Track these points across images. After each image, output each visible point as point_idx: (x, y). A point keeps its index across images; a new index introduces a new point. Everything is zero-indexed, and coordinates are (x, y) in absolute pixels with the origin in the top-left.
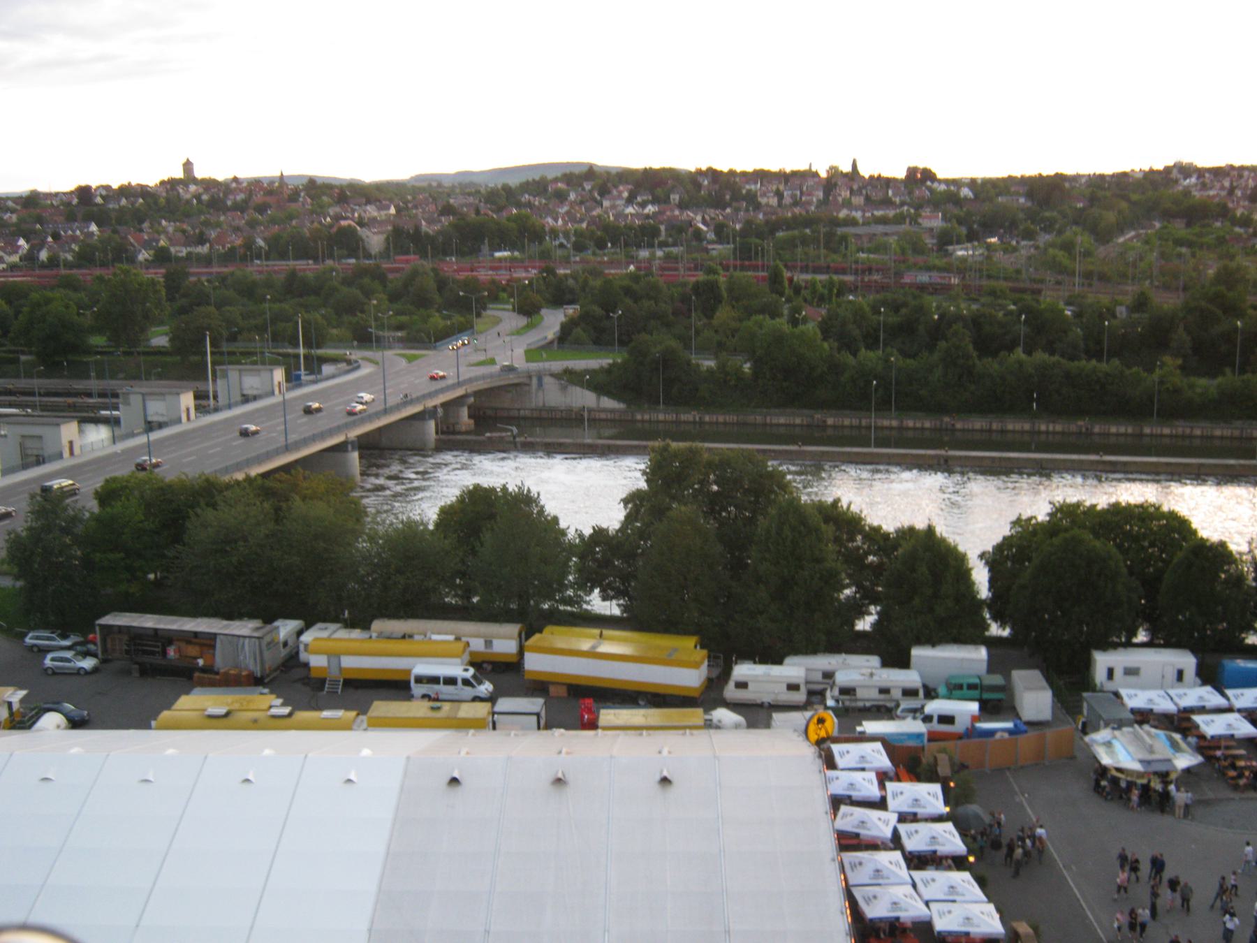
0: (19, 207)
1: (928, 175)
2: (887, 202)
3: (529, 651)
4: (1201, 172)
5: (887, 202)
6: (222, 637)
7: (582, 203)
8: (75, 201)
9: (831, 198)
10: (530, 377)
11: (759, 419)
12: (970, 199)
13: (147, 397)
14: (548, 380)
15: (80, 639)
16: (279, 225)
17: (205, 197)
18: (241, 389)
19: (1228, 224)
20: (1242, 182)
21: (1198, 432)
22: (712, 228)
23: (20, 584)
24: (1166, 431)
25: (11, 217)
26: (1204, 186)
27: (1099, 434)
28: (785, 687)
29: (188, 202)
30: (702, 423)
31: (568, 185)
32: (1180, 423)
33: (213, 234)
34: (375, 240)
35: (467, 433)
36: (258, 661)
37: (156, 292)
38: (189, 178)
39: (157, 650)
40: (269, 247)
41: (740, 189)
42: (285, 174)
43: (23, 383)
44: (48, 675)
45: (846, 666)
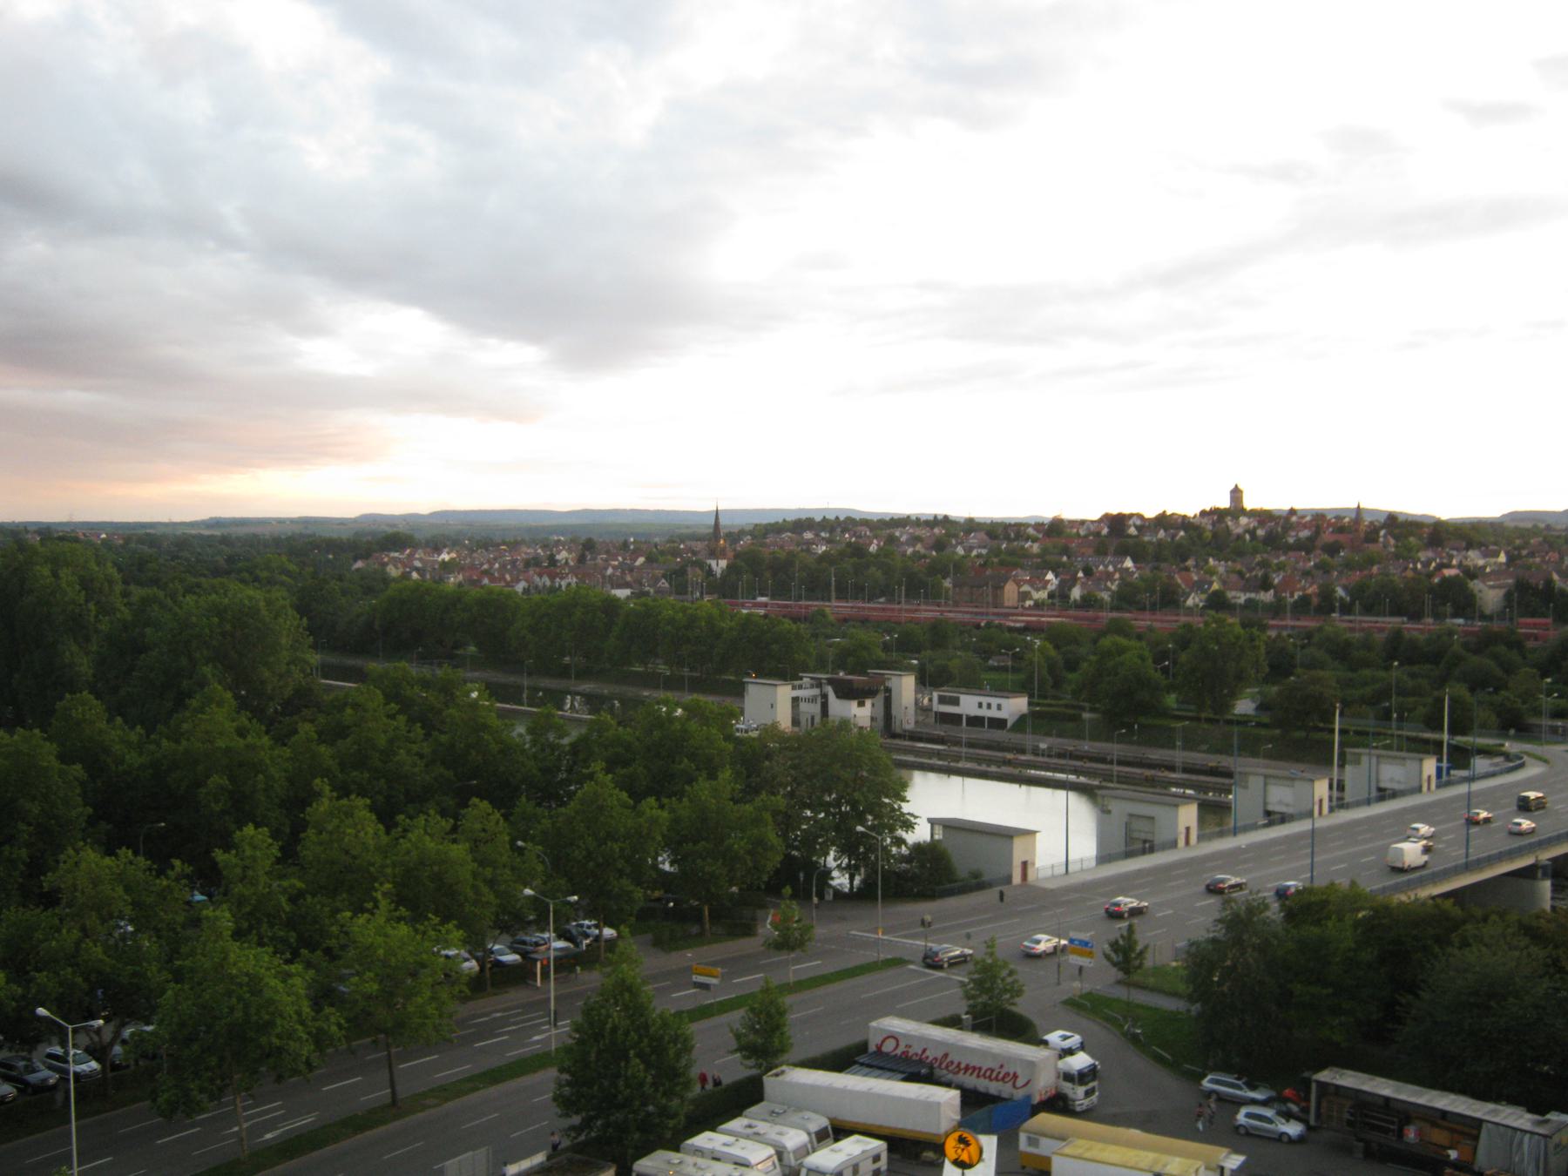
0: (1040, 536)
6: (1489, 1125)
8: (1105, 531)
13: (1272, 781)
15: (1273, 1094)
16: (1361, 570)
17: (1260, 532)
18: (1265, 804)
23: (1196, 1008)
25: (1031, 547)
29: (1239, 537)
33: (1276, 579)
34: (1490, 596)
36: (1541, 1166)
37: (1255, 648)
38: (1237, 509)
39: (1392, 1127)
40: (1352, 596)
42: (1361, 506)
43: (1086, 746)
44: (1238, 1134)
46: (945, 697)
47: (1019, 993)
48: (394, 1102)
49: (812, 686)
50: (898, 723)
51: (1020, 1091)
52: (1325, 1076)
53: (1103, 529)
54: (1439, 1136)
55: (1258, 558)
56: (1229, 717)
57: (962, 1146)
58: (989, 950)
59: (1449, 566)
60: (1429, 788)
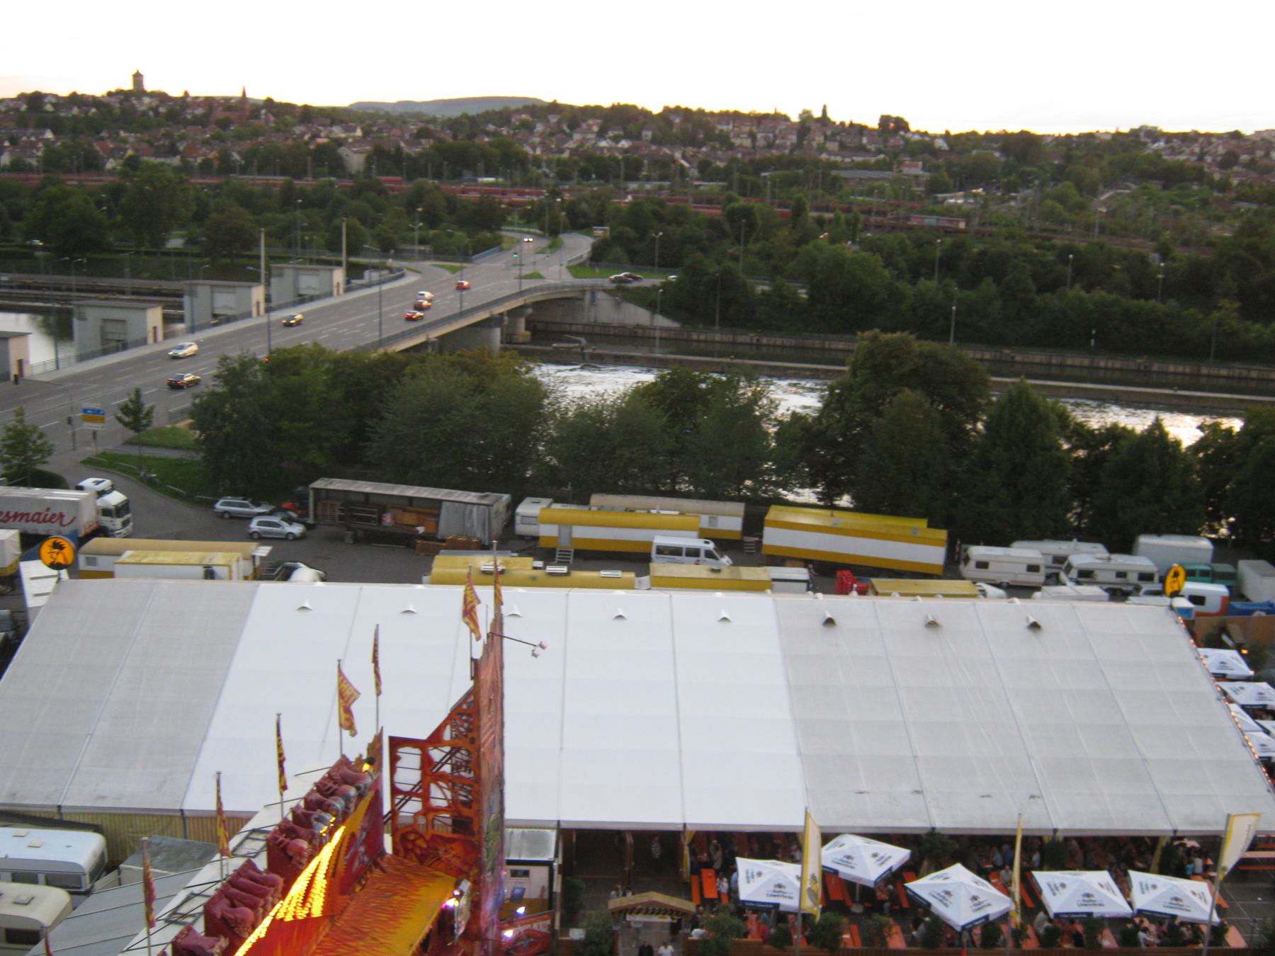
1: (901, 124)
2: (862, 149)
3: (769, 526)
4: (1169, 137)
5: (862, 149)
7: (552, 134)
8: (24, 108)
9: (805, 142)
10: (583, 291)
11: (818, 344)
12: (944, 151)
14: (601, 296)
17: (162, 110)
18: (213, 308)
19: (1206, 187)
20: (1211, 148)
21: (1254, 374)
22: (696, 164)
24: (1224, 372)
26: (1173, 151)
27: (1158, 372)
28: (1025, 567)
29: (144, 114)
30: (759, 345)
31: (532, 115)
32: (1237, 365)
33: (181, 147)
34: (355, 159)
35: (524, 343)
36: (487, 528)
41: (714, 128)
43: (42, 279)
45: (1077, 551)
47: (50, 453)
51: (66, 528)
52: (320, 484)
53: (21, 105)
54: (408, 518)
55: (163, 131)
56: (163, 250)
57: (56, 550)
58: (19, 418)
59: (319, 136)
60: (338, 294)
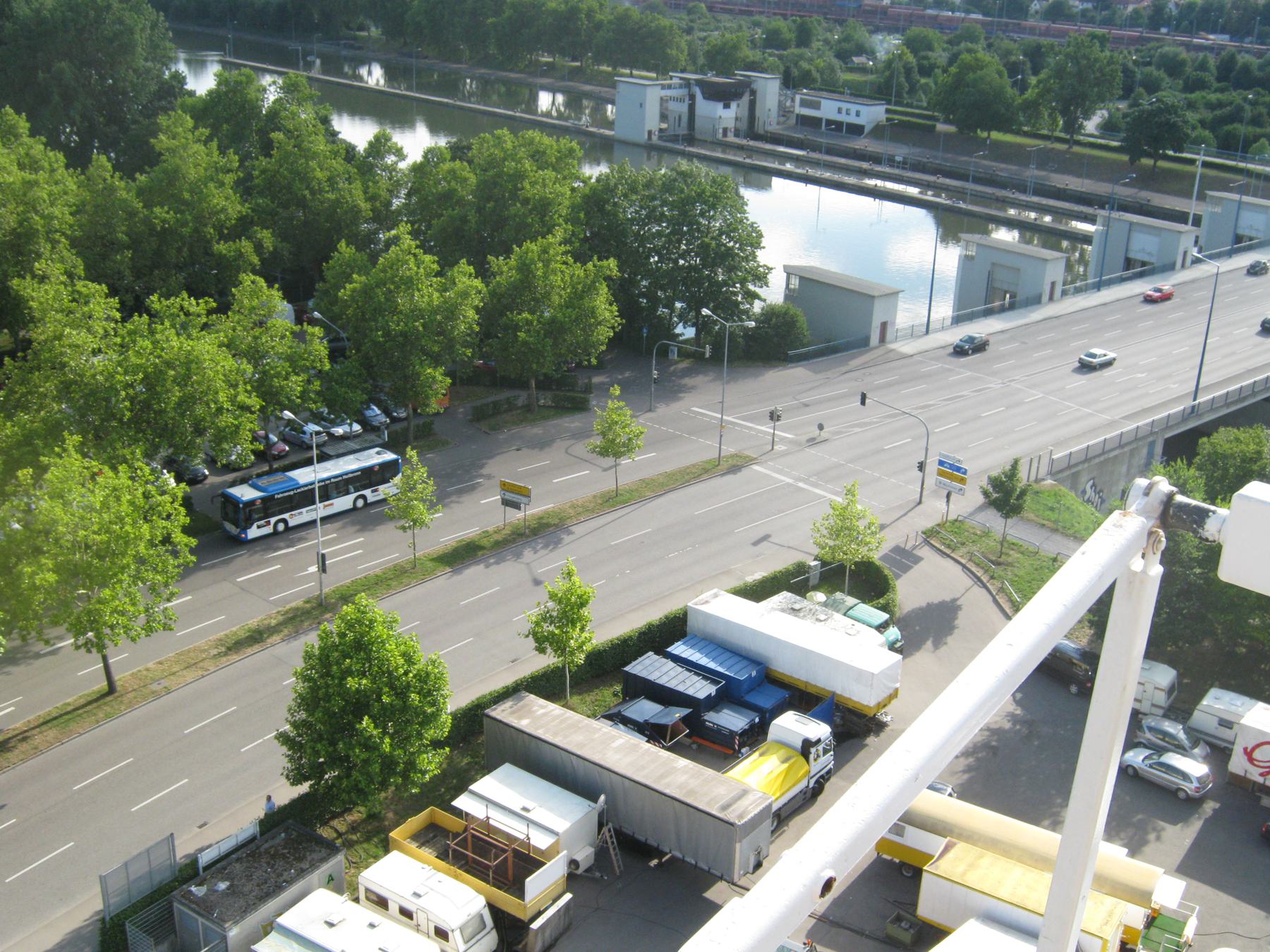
46: (807, 100)
48: (112, 689)
49: (681, 86)
50: (761, 123)
